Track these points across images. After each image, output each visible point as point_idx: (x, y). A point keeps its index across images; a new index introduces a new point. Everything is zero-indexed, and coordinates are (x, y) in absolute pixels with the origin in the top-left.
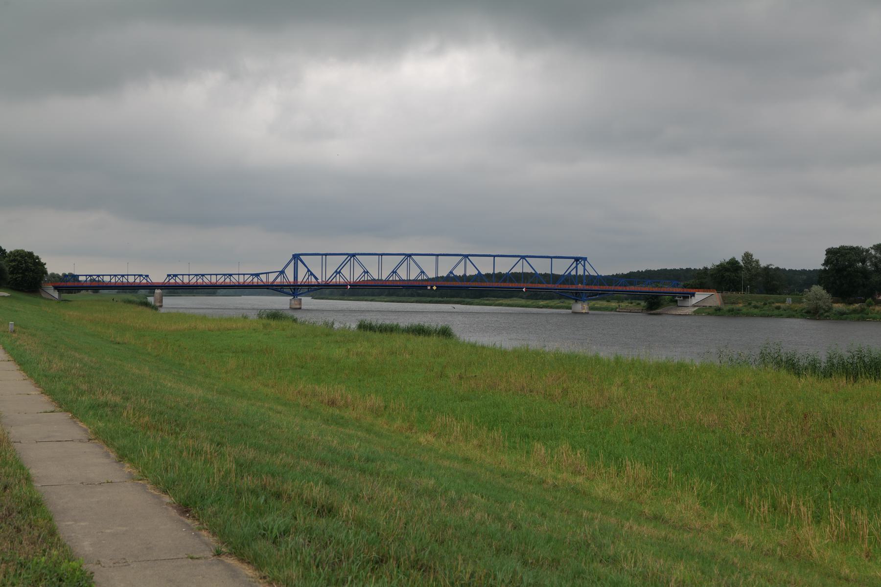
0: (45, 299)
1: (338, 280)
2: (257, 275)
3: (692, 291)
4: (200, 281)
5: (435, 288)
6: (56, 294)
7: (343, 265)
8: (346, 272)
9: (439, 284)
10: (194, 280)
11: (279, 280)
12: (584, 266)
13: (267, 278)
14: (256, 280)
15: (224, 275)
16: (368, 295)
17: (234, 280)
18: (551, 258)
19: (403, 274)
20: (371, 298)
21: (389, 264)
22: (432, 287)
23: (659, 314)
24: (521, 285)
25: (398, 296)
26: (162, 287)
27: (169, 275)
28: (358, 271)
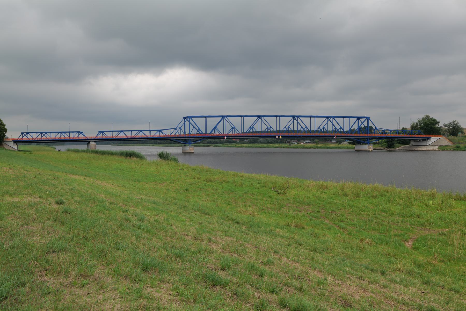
0: (6, 149)
1: (217, 133)
2: (160, 131)
3: (428, 136)
4: (44, 137)
5: (281, 137)
6: (15, 147)
7: (255, 123)
8: (220, 127)
9: (284, 135)
10: (58, 136)
11: (213, 132)
12: (189, 121)
13: (150, 133)
14: (80, 136)
15: (60, 132)
16: (132, 144)
17: (67, 136)
18: (205, 117)
19: (256, 128)
20: (152, 145)
21: (212, 122)
22: (279, 137)
23: (394, 151)
24: (334, 135)
25: (204, 143)
26: (94, 140)
27: (22, 133)
28: (228, 128)
